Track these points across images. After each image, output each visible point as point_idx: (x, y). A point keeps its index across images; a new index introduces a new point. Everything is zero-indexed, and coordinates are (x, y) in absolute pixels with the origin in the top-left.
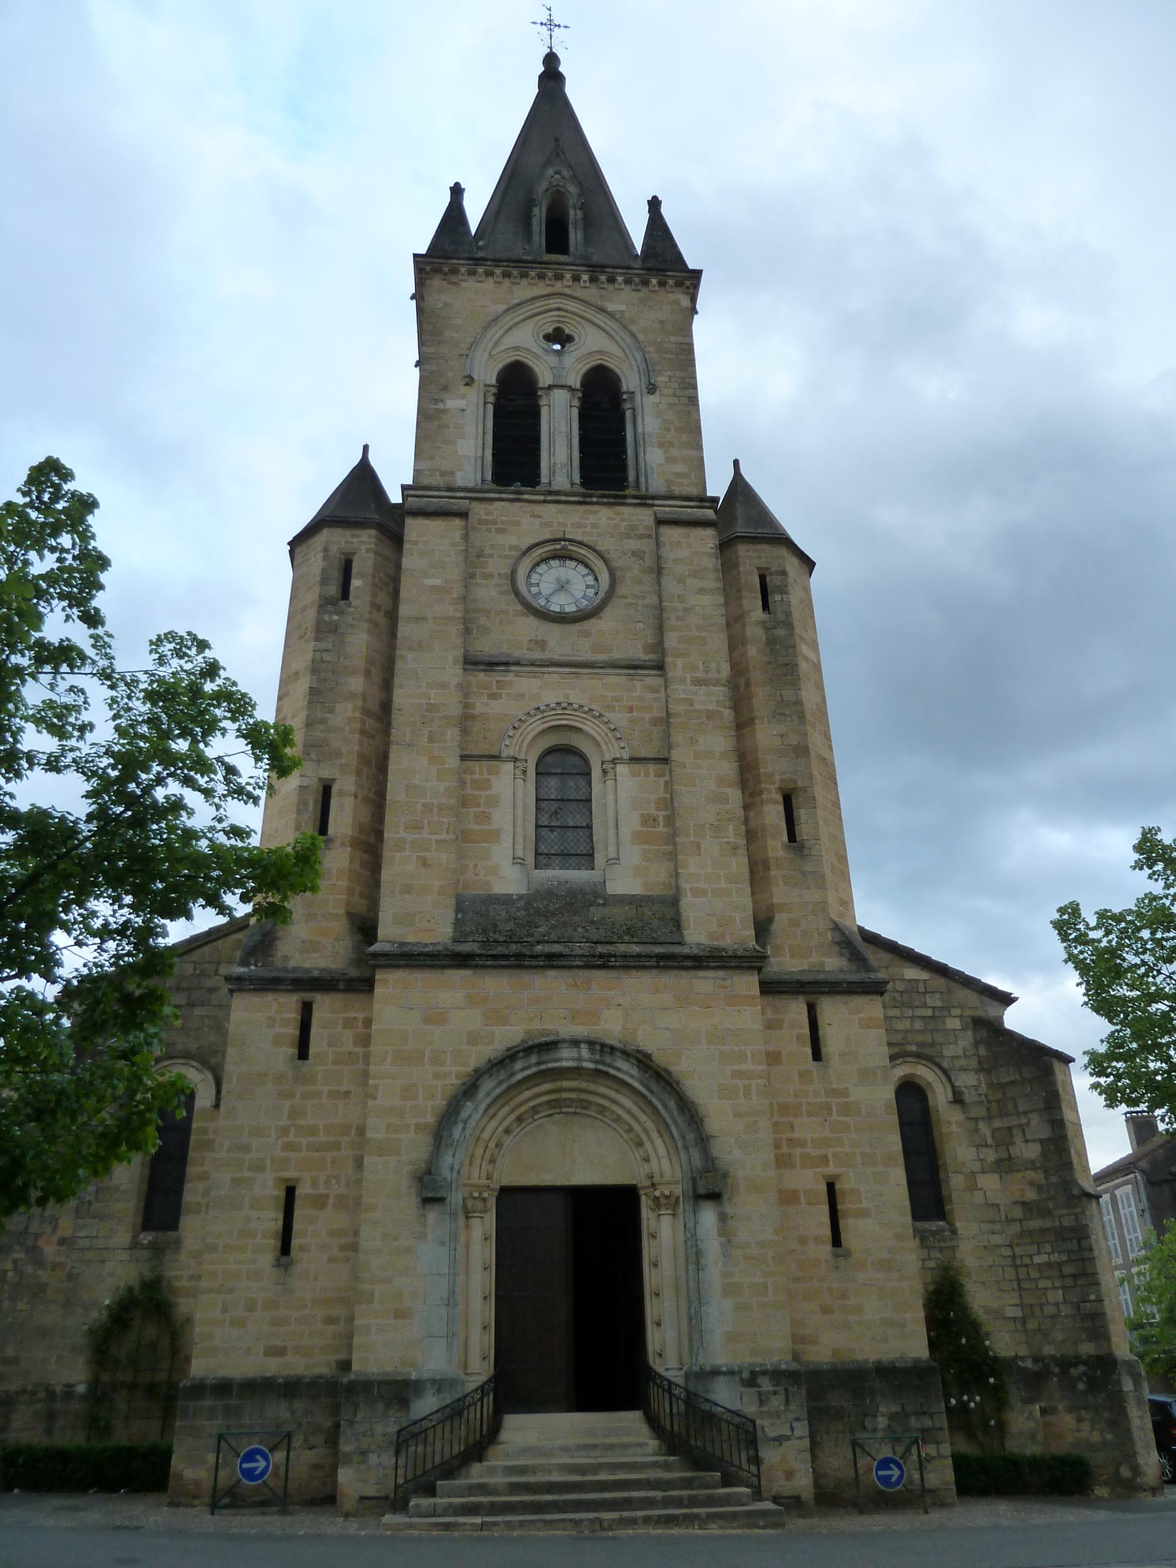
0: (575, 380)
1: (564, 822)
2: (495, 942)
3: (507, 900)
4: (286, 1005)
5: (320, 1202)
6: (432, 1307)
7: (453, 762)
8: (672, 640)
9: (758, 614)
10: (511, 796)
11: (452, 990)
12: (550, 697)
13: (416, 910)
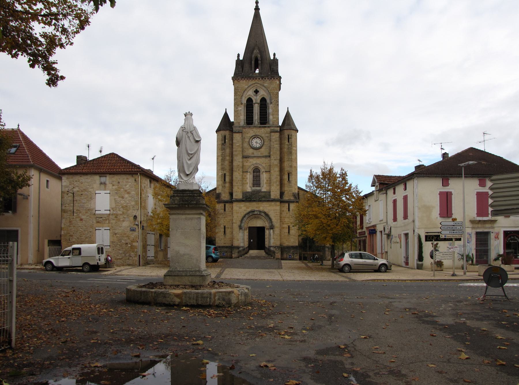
0: (259, 101)
1: (257, 181)
2: (248, 198)
3: (249, 192)
4: (223, 205)
5: (228, 228)
6: (241, 239)
7: (241, 173)
8: (271, 153)
9: (287, 143)
10: (249, 177)
11: (242, 205)
12: (254, 162)
13: (238, 195)
